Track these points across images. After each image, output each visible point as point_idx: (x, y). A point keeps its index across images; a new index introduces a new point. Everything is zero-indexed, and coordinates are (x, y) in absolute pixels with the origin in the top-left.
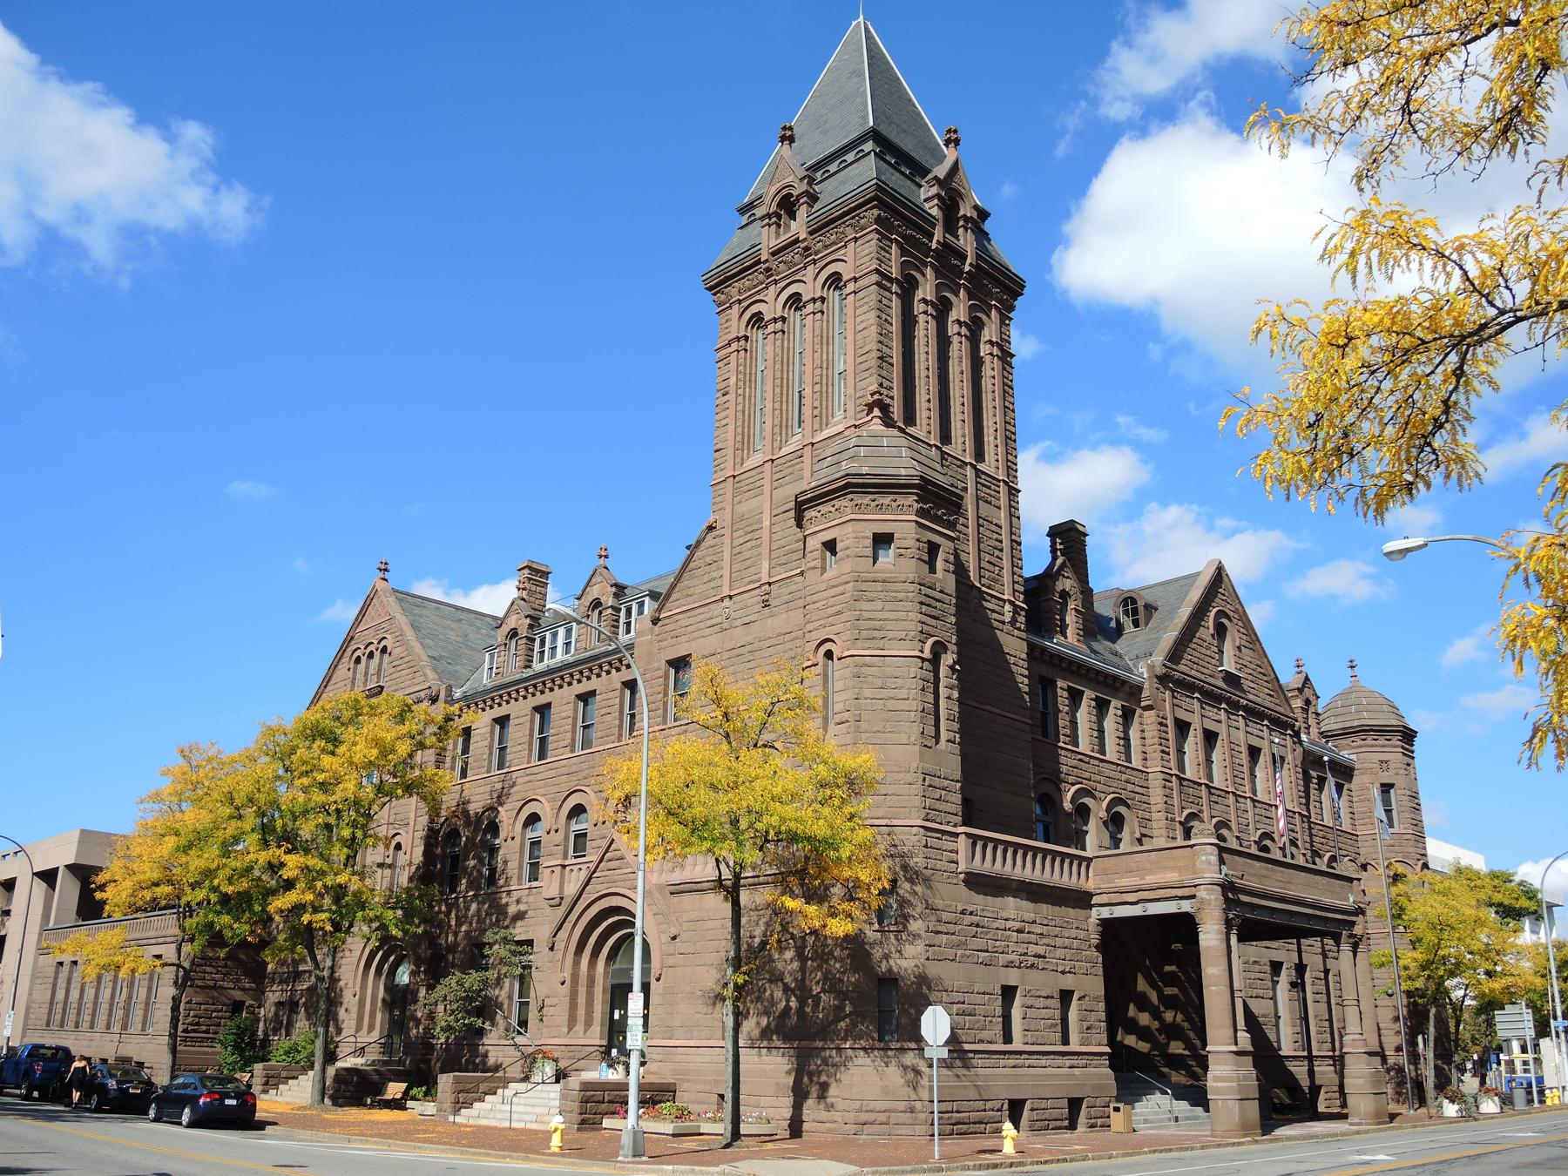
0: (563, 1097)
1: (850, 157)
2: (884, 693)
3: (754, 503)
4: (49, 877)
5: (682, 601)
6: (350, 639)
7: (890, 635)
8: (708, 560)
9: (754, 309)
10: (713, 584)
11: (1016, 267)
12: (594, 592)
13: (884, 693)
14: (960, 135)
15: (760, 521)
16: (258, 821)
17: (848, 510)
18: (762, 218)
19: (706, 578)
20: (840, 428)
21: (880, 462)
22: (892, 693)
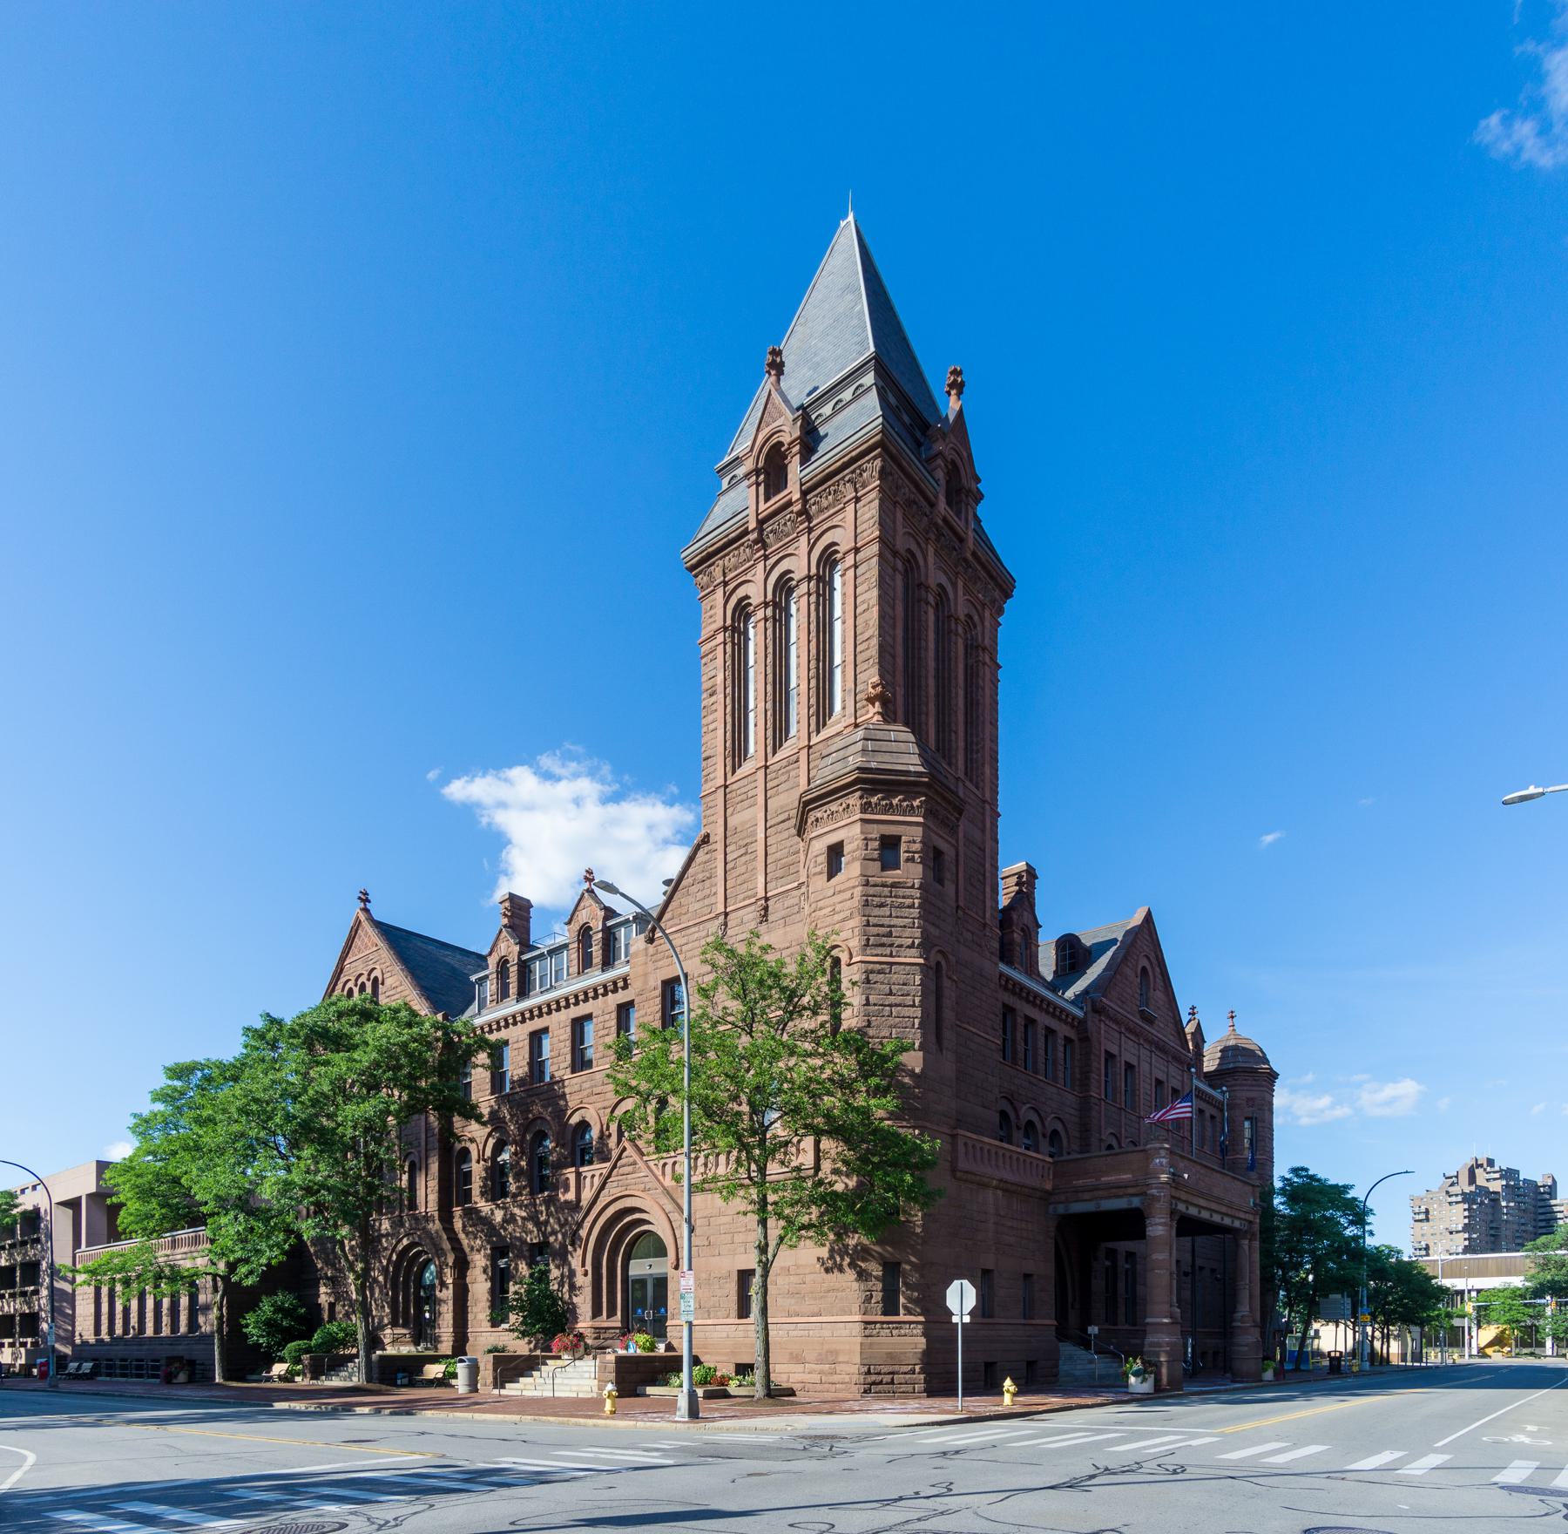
0: (603, 1368)
1: (847, 395)
2: (892, 999)
3: (747, 814)
4: (73, 1204)
5: (676, 921)
6: (339, 970)
7: (898, 942)
8: (700, 876)
9: (740, 593)
10: (707, 902)
11: (1011, 561)
12: (583, 917)
13: (892, 999)
14: (964, 377)
15: (754, 834)
16: (726, 1369)
17: (857, 809)
18: (747, 476)
19: (700, 895)
20: (839, 728)
21: (887, 757)
22: (898, 1000)
